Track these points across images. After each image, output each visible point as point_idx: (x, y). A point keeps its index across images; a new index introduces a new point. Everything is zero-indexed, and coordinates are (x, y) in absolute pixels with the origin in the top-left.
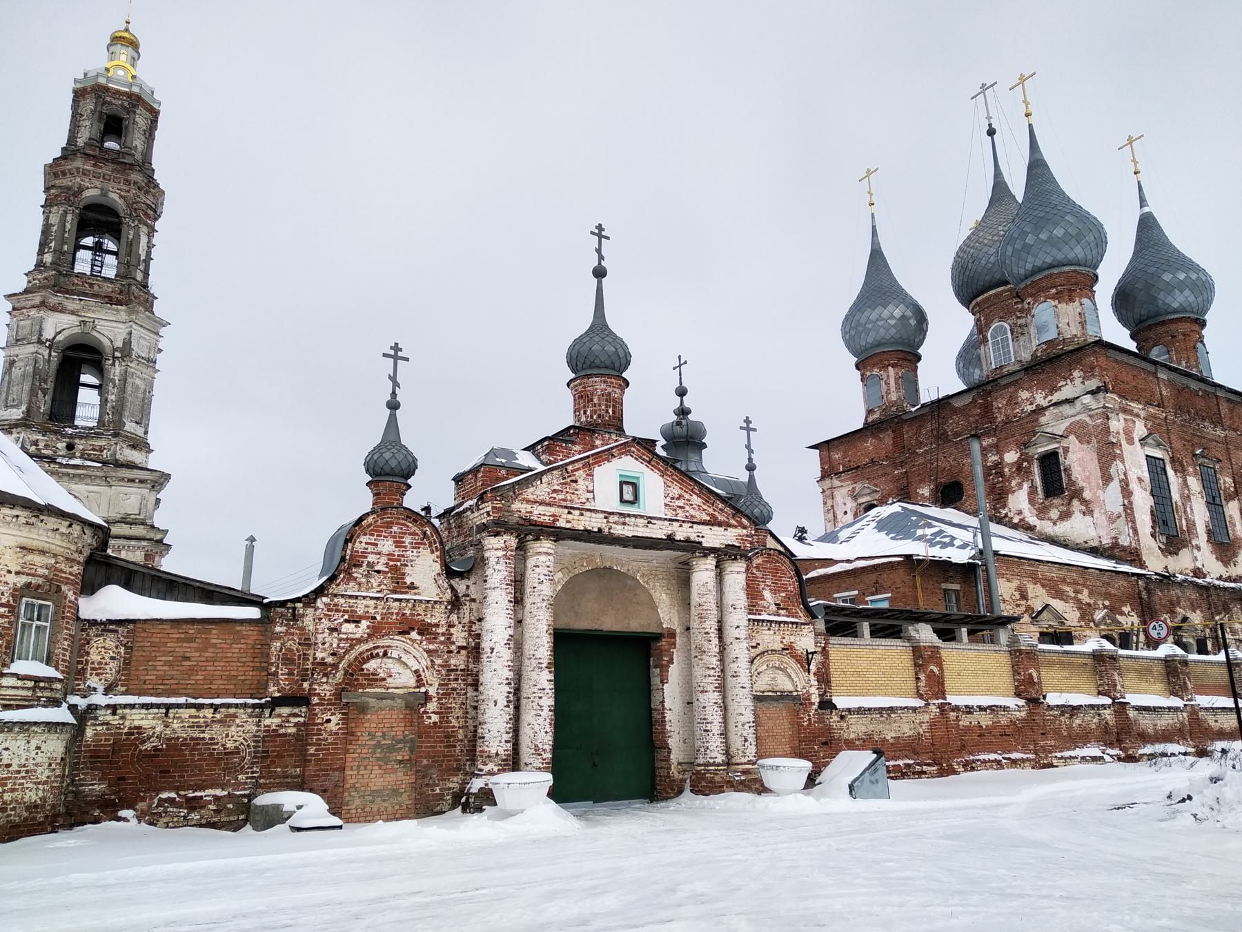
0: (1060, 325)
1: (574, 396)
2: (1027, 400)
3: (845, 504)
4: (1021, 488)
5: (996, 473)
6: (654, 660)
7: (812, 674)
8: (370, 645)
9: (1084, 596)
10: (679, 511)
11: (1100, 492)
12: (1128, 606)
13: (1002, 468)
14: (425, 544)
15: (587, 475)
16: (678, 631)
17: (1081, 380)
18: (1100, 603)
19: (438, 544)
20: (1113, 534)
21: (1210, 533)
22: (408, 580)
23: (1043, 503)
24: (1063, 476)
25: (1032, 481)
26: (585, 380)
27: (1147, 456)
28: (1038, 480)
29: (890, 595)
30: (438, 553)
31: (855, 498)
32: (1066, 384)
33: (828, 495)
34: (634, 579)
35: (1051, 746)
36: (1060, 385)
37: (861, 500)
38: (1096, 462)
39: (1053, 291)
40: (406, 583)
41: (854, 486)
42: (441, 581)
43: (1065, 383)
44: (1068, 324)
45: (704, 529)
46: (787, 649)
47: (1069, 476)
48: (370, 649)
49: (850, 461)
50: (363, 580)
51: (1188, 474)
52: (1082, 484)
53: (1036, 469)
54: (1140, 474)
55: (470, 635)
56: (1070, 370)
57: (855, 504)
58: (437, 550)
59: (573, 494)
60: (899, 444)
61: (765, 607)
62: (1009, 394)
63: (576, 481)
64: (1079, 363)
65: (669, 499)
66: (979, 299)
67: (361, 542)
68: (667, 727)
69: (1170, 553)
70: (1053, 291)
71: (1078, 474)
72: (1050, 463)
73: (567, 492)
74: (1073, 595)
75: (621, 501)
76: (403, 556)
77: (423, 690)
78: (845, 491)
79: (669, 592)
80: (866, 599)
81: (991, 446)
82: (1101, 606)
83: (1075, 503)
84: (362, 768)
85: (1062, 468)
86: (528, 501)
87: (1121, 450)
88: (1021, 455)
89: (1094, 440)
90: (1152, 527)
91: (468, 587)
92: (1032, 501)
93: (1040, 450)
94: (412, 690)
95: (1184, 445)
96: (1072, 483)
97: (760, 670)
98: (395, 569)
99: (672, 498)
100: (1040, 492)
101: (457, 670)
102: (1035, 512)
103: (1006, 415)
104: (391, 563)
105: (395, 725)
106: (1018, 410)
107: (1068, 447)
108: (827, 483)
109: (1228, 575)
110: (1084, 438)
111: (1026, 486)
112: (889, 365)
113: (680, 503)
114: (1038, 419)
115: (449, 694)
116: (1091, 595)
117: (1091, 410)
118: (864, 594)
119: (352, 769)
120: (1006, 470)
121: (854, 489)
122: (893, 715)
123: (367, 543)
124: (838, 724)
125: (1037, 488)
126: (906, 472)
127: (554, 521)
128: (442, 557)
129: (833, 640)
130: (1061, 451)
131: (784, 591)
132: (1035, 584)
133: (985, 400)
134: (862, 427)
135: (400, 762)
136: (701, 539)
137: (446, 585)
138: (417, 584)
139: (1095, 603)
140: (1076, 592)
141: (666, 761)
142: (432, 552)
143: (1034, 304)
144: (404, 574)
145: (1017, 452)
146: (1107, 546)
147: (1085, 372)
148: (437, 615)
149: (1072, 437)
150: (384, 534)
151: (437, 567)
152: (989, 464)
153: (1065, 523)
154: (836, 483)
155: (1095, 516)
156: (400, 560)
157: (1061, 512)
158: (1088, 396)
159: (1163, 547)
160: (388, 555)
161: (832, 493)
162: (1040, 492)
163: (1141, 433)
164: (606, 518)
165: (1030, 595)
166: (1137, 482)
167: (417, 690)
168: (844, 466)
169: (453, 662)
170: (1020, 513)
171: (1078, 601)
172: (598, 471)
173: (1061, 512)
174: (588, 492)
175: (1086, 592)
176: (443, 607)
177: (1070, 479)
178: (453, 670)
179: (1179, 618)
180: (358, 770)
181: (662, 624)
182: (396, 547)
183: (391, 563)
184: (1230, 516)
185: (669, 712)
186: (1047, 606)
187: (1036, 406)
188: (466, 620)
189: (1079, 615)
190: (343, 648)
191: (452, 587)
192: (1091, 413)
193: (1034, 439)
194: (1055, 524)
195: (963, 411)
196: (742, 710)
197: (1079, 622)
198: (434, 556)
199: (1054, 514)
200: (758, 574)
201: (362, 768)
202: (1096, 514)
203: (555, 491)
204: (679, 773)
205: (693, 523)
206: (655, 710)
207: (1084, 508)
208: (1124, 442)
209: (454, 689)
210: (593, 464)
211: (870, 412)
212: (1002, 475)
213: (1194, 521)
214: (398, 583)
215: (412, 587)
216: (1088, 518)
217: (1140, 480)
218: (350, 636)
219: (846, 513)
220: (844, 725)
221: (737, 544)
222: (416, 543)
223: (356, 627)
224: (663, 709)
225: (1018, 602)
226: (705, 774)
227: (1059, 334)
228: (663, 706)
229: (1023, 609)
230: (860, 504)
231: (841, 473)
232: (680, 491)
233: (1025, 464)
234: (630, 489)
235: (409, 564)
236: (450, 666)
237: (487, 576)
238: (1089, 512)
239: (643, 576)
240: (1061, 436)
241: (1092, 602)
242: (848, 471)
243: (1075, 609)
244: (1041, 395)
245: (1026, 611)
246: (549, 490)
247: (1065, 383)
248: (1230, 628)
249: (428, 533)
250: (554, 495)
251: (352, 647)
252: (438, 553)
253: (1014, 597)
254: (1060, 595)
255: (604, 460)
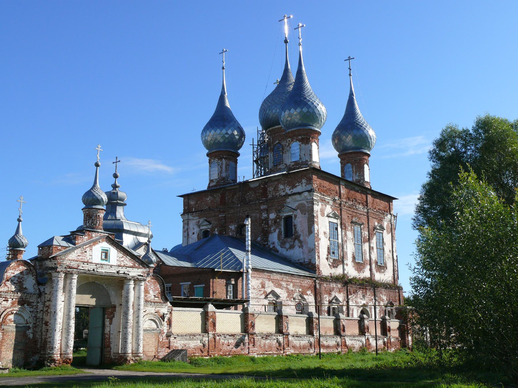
0: (301, 155)
1: (84, 214)
2: (282, 189)
3: (194, 229)
4: (275, 232)
5: (265, 223)
6: (107, 316)
7: (165, 322)
8: (12, 309)
9: (291, 287)
10: (122, 262)
11: (307, 238)
12: (310, 291)
13: (268, 221)
14: (30, 273)
15: (90, 249)
16: (117, 306)
17: (305, 184)
18: (297, 290)
19: (35, 273)
20: (310, 258)
21: (354, 258)
22: (24, 286)
23: (284, 240)
24: (293, 228)
25: (280, 229)
26: (90, 210)
27: (329, 222)
28: (283, 228)
29: (204, 285)
30: (35, 277)
31: (199, 226)
32: (299, 185)
33: (186, 223)
34: (102, 286)
35: (256, 350)
36: (296, 185)
37: (202, 228)
38: (307, 223)
39: (300, 137)
40: (23, 287)
41: (199, 220)
42: (35, 287)
43: (298, 184)
44: (304, 155)
45: (130, 269)
46: (157, 312)
47: (295, 228)
48: (11, 311)
49: (198, 206)
50: (10, 286)
51: (348, 230)
52: (300, 233)
53: (282, 223)
54: (325, 230)
55: (44, 306)
56: (301, 179)
57: (198, 230)
58: (34, 276)
59: (85, 256)
60: (223, 201)
61: (149, 297)
62: (275, 185)
63: (86, 252)
64: (305, 176)
65: (118, 258)
66: (271, 129)
67: (9, 273)
68: (111, 340)
69: (334, 267)
70: (300, 137)
71: (299, 228)
72: (288, 220)
73: (83, 256)
74: (285, 286)
75: (101, 259)
76: (23, 277)
77: (28, 325)
78: (194, 222)
79: (114, 291)
80: (194, 286)
81: (264, 209)
82: (298, 291)
83: (297, 242)
84: (7, 351)
85: (293, 224)
86: (69, 260)
87: (318, 220)
88: (277, 215)
89: (307, 214)
90: (327, 255)
91: (44, 289)
92: (279, 238)
93: (285, 215)
94: (24, 325)
95: (348, 217)
96: (296, 232)
97: (146, 320)
98: (20, 282)
99: (120, 258)
100: (283, 235)
101: (39, 318)
102: (280, 243)
103: (272, 195)
104: (19, 280)
105: (18, 337)
106: (278, 194)
107: (296, 215)
108: (186, 216)
109: (359, 277)
110: (303, 212)
111: (277, 231)
112: (223, 158)
113: (122, 259)
114: (285, 200)
115: (37, 327)
116: (294, 286)
117: (307, 199)
118: (193, 284)
119: (4, 352)
120: (270, 222)
121: (199, 221)
122: (194, 338)
123: (11, 273)
124: (173, 340)
125: (282, 232)
126: (225, 216)
127: (78, 267)
128: (36, 278)
129: (174, 308)
130: (293, 216)
131: (157, 291)
132: (269, 281)
133: (264, 186)
134: (205, 188)
135: (20, 350)
136: (129, 273)
137: (37, 288)
138: (27, 287)
139: (295, 290)
140: (287, 285)
141: (109, 352)
142: (33, 276)
143: (291, 142)
144: (23, 284)
145: (275, 214)
146: (307, 263)
147: (307, 181)
148: (34, 299)
149: (299, 211)
150: (17, 269)
151: (34, 282)
152: (262, 218)
153: (291, 250)
154: (191, 217)
155: (304, 249)
156: (22, 279)
157: (290, 245)
158: (307, 193)
159: (331, 264)
160: (18, 277)
161: (188, 222)
162: (283, 235)
163: (328, 211)
164: (96, 265)
165: (266, 286)
166: (323, 234)
167: (26, 325)
168: (195, 209)
169: (38, 315)
170: (273, 243)
171: (287, 288)
172: (94, 248)
173: (290, 245)
174: (90, 256)
175: (292, 285)
176: (36, 296)
177: (296, 230)
178: (38, 319)
179: (333, 296)
180: (6, 352)
181: (111, 303)
182: (21, 274)
183: (19, 280)
184: (365, 250)
185: (112, 335)
186: (272, 291)
187: (286, 193)
188: (43, 301)
189: (287, 295)
190: (2, 310)
191: (39, 289)
192: (308, 201)
193: (283, 209)
194: (287, 250)
195: (254, 189)
196: (74, 285)
197: (287, 298)
198: (33, 278)
199: (287, 246)
200: (149, 284)
201: (7, 351)
202: (304, 248)
203: (79, 256)
204: (114, 356)
205: (127, 267)
206: (106, 334)
207: (300, 244)
208: (319, 215)
209: (38, 325)
210: (92, 245)
211: (211, 181)
212: (268, 224)
213: (347, 252)
214: (21, 287)
215: (26, 288)
216: (301, 249)
217: (325, 233)
218: (5, 306)
219: (194, 233)
220: (175, 340)
221: (142, 275)
222: (27, 273)
223: (7, 303)
224: (110, 334)
225: (260, 289)
226: (124, 356)
227: (300, 159)
228: (110, 332)
229: (262, 292)
230: (201, 230)
231: (193, 212)
232: (122, 255)
233: (278, 220)
234: (106, 254)
235: (25, 280)
236: (37, 317)
237: (54, 286)
238: (301, 246)
239: (106, 285)
240: (294, 209)
241: (294, 289)
242: (197, 212)
243: (285, 292)
244: (288, 188)
245: (264, 293)
246: (76, 255)
247: (298, 184)
248: (355, 301)
249: (32, 269)
250: (78, 257)
251: (5, 310)
252: (35, 277)
253: (259, 287)
254: (280, 286)
255: (96, 244)
